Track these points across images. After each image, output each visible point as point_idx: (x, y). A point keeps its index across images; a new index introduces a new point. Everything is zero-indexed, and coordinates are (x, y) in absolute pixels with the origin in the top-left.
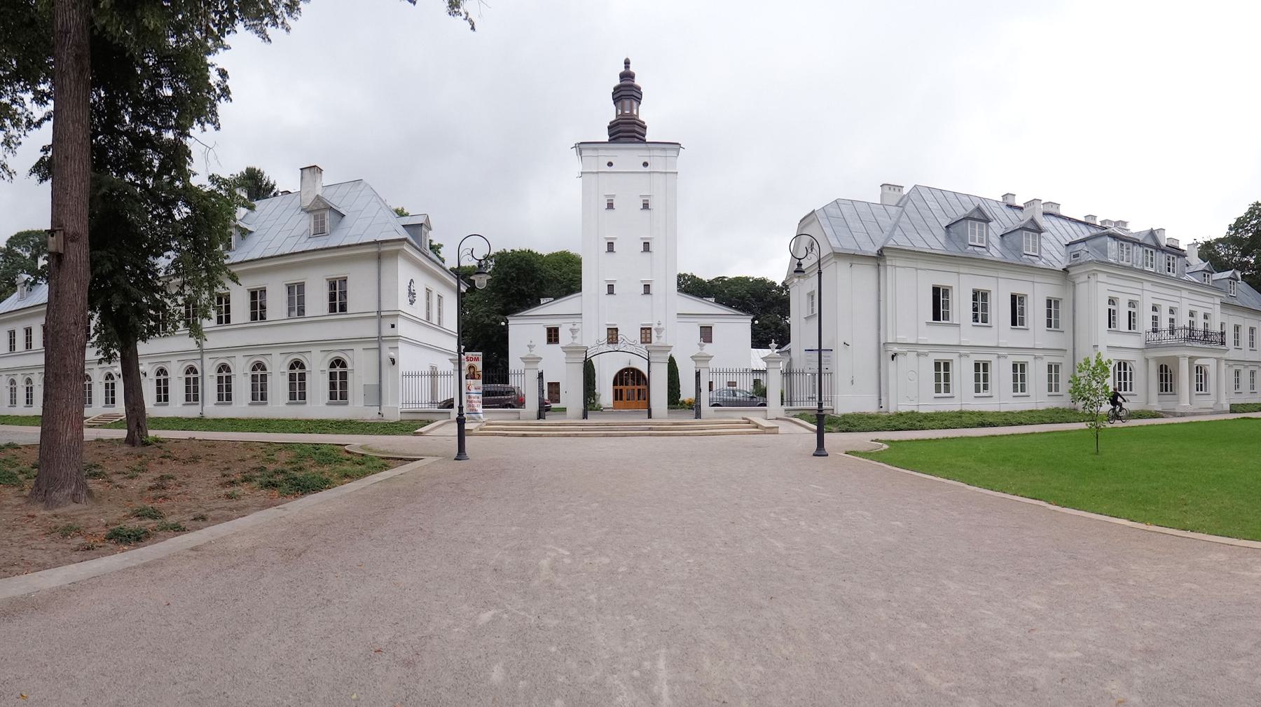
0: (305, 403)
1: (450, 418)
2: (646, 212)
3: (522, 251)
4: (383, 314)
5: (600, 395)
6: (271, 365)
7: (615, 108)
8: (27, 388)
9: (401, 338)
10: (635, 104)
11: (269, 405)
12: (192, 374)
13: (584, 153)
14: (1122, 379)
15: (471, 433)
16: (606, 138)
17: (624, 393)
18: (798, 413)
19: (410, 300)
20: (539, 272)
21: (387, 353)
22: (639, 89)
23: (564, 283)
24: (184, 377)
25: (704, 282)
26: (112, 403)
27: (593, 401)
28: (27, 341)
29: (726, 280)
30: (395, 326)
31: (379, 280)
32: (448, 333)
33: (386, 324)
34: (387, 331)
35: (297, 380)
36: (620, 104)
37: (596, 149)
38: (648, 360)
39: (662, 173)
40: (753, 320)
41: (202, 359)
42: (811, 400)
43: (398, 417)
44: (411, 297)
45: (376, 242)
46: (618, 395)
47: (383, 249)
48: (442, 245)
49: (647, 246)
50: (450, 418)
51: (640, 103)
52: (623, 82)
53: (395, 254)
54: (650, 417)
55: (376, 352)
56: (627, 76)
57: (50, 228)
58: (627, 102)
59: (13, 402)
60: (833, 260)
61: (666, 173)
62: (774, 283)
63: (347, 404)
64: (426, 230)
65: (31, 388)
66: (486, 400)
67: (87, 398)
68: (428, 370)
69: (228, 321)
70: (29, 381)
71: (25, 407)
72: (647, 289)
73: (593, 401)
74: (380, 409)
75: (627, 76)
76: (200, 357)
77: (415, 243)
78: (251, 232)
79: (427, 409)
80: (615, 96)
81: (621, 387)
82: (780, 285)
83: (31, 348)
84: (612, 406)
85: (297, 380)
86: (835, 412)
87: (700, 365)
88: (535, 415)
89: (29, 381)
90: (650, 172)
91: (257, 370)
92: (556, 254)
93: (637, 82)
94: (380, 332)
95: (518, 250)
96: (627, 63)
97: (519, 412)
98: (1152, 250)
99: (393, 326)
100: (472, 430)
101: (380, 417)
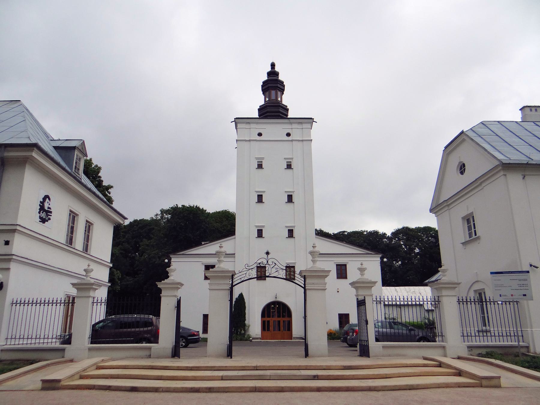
2: (289, 171)
3: (190, 207)
5: (249, 326)
7: (264, 97)
10: (279, 93)
13: (239, 126)
15: (57, 385)
16: (257, 116)
17: (271, 324)
18: (484, 351)
19: (40, 218)
20: (204, 223)
22: (282, 82)
23: (224, 234)
25: (331, 234)
27: (243, 332)
29: (346, 233)
30: (10, 243)
32: (99, 262)
36: (267, 93)
37: (249, 123)
38: (304, 288)
39: (299, 141)
40: (382, 258)
42: (481, 334)
46: (265, 326)
48: (112, 187)
49: (290, 199)
50: (63, 357)
51: (283, 94)
52: (270, 78)
53: (23, 162)
54: (307, 355)
56: (273, 74)
58: (273, 92)
60: (502, 173)
61: (302, 141)
62: (385, 234)
64: (80, 155)
66: (287, 316)
72: (291, 233)
73: (243, 332)
75: (273, 74)
80: (263, 88)
81: (268, 319)
82: (390, 236)
84: (260, 336)
86: (532, 349)
87: (362, 292)
88: (169, 352)
90: (292, 141)
92: (219, 212)
93: (281, 78)
95: (188, 206)
96: (273, 65)
97: (150, 349)
100: (59, 381)
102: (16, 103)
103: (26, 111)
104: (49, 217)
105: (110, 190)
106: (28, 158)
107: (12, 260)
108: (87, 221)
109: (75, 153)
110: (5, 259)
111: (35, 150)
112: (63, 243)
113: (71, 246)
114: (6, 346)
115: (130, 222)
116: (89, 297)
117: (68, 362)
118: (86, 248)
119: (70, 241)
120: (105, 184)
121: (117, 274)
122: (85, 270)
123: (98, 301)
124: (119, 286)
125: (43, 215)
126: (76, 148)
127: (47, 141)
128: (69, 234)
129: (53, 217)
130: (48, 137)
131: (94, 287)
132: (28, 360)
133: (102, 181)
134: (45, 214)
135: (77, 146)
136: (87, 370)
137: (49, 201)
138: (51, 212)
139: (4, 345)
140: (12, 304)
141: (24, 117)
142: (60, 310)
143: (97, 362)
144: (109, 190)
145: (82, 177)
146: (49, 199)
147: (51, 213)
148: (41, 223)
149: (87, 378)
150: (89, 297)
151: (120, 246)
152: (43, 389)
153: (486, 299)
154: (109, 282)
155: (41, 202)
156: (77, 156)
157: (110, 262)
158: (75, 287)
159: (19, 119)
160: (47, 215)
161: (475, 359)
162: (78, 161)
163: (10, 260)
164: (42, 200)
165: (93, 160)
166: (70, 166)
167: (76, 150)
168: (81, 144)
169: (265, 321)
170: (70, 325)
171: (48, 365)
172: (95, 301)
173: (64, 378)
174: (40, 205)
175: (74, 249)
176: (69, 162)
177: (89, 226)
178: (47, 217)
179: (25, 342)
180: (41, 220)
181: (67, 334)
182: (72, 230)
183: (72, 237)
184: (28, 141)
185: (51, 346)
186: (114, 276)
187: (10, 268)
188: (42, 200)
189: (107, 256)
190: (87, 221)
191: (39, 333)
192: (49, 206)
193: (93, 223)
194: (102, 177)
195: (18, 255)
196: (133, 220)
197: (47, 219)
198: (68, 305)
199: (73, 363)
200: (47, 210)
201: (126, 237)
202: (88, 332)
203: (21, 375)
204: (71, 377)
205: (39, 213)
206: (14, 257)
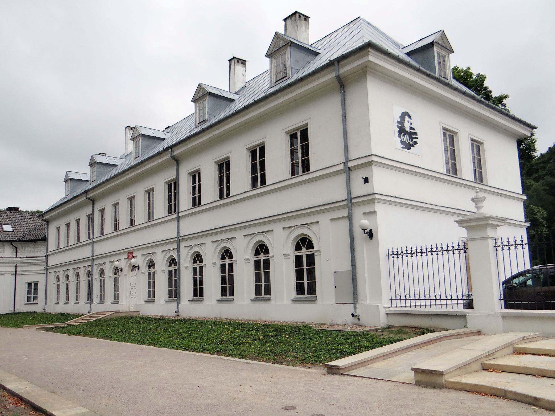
0: (269, 299)
1: (465, 327)
4: (351, 164)
6: (319, 239)
8: (170, 272)
9: (377, 196)
11: (273, 302)
12: (304, 249)
14: (90, 295)
15: (438, 380)
19: (402, 142)
24: (219, 262)
31: (344, 117)
34: (359, 189)
35: (152, 279)
41: (179, 249)
43: (382, 321)
47: (342, 71)
48: (506, 97)
50: (465, 327)
55: (346, 222)
59: (152, 294)
63: (314, 300)
64: (442, 52)
71: (294, 301)
74: (355, 308)
76: (90, 264)
79: (408, 309)
85: (152, 279)
89: (172, 261)
98: (481, 134)
99: (366, 180)
100: (440, 374)
101: (355, 320)
103: (364, 22)
104: (414, 140)
105: (504, 102)
107: (376, 200)
108: (473, 140)
111: (371, 52)
112: (443, 173)
113: (456, 176)
114: (391, 309)
115: (550, 148)
116: (487, 238)
117: (473, 334)
120: (495, 94)
121: (539, 211)
123: (514, 248)
124: (546, 227)
127: (398, 50)
128: (450, 161)
132: (420, 328)
133: (491, 92)
134: (408, 137)
136: (493, 355)
137: (409, 120)
138: (416, 134)
139: (389, 308)
143: (513, 341)
144: (503, 103)
147: (417, 135)
148: (405, 150)
149: (495, 371)
150: (487, 238)
151: (541, 181)
152: (418, 383)
154: (526, 221)
155: (398, 122)
156: (438, 54)
157: (521, 193)
163: (373, 201)
164: (399, 120)
165: (471, 68)
167: (435, 47)
168: (441, 36)
169: (221, 275)
170: (171, 301)
171: (440, 339)
172: (499, 243)
173: (448, 369)
175: (462, 179)
176: (430, 64)
178: (412, 140)
179: (413, 304)
180: (404, 146)
183: (455, 164)
185: (446, 310)
186: (535, 214)
187: (376, 210)
188: (399, 120)
190: (473, 140)
192: (412, 126)
193: (482, 141)
194: (489, 87)
195: (381, 193)
196: (553, 145)
197: (412, 143)
199: (481, 336)
200: (409, 131)
201: (547, 169)
202: (497, 292)
203: (398, 353)
204: (464, 367)
206: (377, 196)
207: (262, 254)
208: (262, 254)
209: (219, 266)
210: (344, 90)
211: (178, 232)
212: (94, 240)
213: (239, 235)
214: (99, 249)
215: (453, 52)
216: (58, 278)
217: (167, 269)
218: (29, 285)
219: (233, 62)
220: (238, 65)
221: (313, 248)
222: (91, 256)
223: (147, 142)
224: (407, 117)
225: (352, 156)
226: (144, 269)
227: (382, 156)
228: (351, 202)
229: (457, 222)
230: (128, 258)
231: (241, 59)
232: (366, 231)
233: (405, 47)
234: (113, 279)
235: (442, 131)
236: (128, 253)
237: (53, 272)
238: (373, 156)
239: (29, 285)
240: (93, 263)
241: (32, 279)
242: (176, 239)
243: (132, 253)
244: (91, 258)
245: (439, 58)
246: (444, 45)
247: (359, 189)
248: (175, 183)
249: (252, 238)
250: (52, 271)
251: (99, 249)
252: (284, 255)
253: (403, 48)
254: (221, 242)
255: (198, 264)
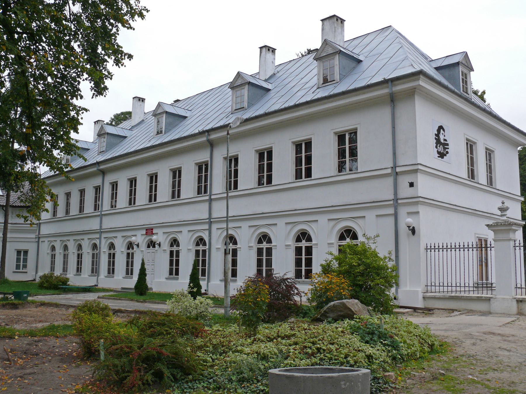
4: (398, 170)
9: (421, 199)
19: (439, 153)
21: (406, 220)
24: (255, 246)
26: (176, 275)
28: (151, 191)
30: (415, 184)
31: (394, 127)
33: (403, 182)
44: (441, 149)
45: (385, 82)
53: (411, 94)
55: (392, 220)
57: (317, 44)
64: (465, 71)
65: (178, 252)
67: (200, 268)
68: (472, 240)
69: (309, 174)
70: (112, 246)
76: (98, 237)
77: (450, 86)
78: (362, 61)
83: (134, 204)
91: (301, 241)
94: (396, 193)
102: (388, 30)
104: (446, 150)
106: (415, 88)
108: (487, 149)
109: (459, 70)
110: (345, 209)
118: (490, 181)
119: (472, 174)
122: (501, 209)
125: (441, 149)
126: (460, 63)
129: (451, 149)
130: (426, 58)
131: (513, 228)
135: (460, 60)
137: (443, 132)
140: (427, 249)
141: (400, 43)
142: (473, 255)
145: (472, 97)
146: (444, 130)
148: (440, 158)
153: (486, 245)
155: (436, 134)
156: (462, 72)
158: (491, 229)
159: (396, 46)
160: (445, 149)
161: (52, 291)
162: (465, 79)
164: (436, 133)
166: (457, 86)
167: (460, 66)
168: (465, 57)
172: (517, 244)
174: (435, 138)
175: (478, 183)
177: (489, 153)
178: (445, 150)
181: (484, 281)
182: (471, 162)
184: (410, 70)
188: (436, 133)
189: (517, 190)
190: (487, 149)
191: (441, 281)
192: (445, 138)
193: (494, 150)
197: (445, 153)
198: (482, 250)
205: (436, 147)
207: (201, 246)
208: (201, 246)
209: (168, 253)
210: (394, 104)
211: (210, 214)
212: (103, 213)
213: (281, 222)
214: (109, 223)
215: (473, 71)
216: (53, 248)
217: (193, 248)
218: (19, 252)
219: (264, 49)
220: (269, 53)
221: (272, 243)
222: (99, 228)
223: (171, 119)
224: (442, 130)
225: (400, 162)
226: (166, 246)
227: (425, 165)
228: (397, 202)
229: (488, 225)
230: (146, 234)
231: (271, 48)
232: (410, 228)
233: (433, 60)
234: (91, 255)
235: (466, 141)
236: (147, 230)
237: (46, 242)
238: (419, 165)
239: (19, 252)
240: (101, 236)
241: (22, 247)
242: (208, 220)
243: (152, 229)
244: (99, 231)
245: (462, 75)
246: (466, 64)
247: (405, 191)
248: (207, 165)
249: (295, 226)
250: (46, 240)
251: (109, 223)
252: (328, 243)
253: (430, 61)
254: (259, 228)
255: (175, 248)
